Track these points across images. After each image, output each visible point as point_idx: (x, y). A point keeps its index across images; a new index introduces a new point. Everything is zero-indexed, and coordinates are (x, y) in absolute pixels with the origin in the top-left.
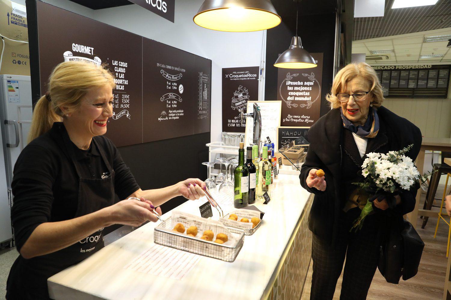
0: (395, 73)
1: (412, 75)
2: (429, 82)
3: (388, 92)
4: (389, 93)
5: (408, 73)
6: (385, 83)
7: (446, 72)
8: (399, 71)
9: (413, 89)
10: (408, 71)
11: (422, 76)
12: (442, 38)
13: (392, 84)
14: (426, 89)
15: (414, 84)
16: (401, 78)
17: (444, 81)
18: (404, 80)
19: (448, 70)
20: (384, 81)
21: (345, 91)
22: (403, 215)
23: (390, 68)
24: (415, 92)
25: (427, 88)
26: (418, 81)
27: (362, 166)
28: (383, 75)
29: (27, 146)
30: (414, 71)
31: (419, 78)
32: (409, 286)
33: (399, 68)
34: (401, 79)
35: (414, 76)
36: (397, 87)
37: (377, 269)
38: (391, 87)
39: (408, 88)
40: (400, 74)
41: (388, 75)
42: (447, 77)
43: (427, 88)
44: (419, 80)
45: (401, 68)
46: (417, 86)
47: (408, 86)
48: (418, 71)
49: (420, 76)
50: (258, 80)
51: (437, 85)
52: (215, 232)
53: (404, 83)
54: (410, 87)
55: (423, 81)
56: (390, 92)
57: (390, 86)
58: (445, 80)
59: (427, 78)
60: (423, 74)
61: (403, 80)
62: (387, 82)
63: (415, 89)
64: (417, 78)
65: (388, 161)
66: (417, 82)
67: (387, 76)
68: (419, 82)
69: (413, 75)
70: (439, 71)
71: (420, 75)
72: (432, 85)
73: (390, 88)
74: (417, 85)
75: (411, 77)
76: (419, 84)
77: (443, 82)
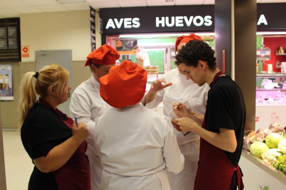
12: (183, 61)
17: (13, 41)
21: (146, 70)
22: (99, 60)
25: (8, 49)
36: (6, 48)
43: (8, 49)
52: (69, 2)
68: (9, 41)
70: (7, 30)
72: (3, 46)
77: (13, 42)
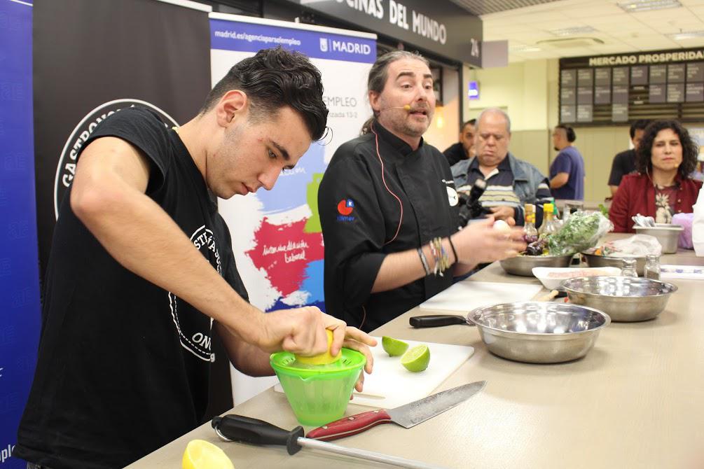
4: (630, 115)
5: (664, 71)
7: (697, 69)
11: (694, 75)
13: (565, 99)
14: (665, 106)
16: (579, 85)
18: (659, 85)
26: (685, 87)
30: (677, 66)
31: (688, 80)
32: (546, 247)
35: (677, 77)
37: (213, 86)
38: (597, 102)
39: (667, 103)
40: (577, 77)
41: (623, 76)
48: (665, 66)
49: (690, 76)
50: (297, 19)
55: (696, 86)
57: (594, 100)
66: (685, 91)
67: (569, 81)
69: (675, 73)
70: (577, 73)
73: (594, 105)
74: (685, 96)
76: (618, 94)
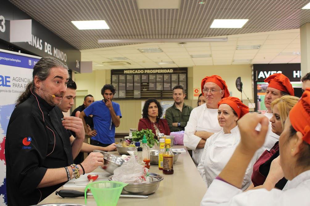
0: (145, 77)
1: (159, 78)
2: (172, 85)
3: (140, 94)
4: (141, 95)
6: (137, 86)
8: (148, 75)
9: (161, 91)
10: (162, 75)
15: (161, 86)
18: (153, 83)
19: (186, 74)
20: (136, 84)
23: (140, 72)
24: (163, 94)
27: (4, 195)
28: (135, 78)
29: (14, 110)
30: (160, 75)
33: (148, 72)
34: (128, 82)
35: (160, 80)
38: (127, 89)
41: (138, 78)
42: (185, 80)
44: (164, 83)
45: (149, 72)
46: (163, 88)
47: (156, 88)
49: (165, 80)
51: (163, 88)
53: (153, 86)
54: (157, 89)
55: (167, 84)
56: (127, 94)
58: (184, 83)
59: (170, 81)
60: (167, 78)
61: (174, 83)
62: (130, 85)
63: (163, 91)
64: (162, 81)
65: (3, 199)
66: (163, 85)
68: (164, 85)
69: (160, 78)
71: (164, 78)
73: (126, 91)
75: (158, 81)
